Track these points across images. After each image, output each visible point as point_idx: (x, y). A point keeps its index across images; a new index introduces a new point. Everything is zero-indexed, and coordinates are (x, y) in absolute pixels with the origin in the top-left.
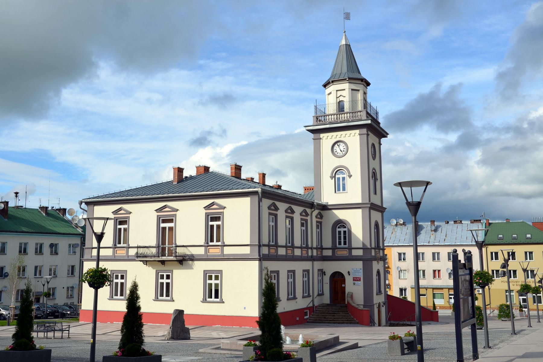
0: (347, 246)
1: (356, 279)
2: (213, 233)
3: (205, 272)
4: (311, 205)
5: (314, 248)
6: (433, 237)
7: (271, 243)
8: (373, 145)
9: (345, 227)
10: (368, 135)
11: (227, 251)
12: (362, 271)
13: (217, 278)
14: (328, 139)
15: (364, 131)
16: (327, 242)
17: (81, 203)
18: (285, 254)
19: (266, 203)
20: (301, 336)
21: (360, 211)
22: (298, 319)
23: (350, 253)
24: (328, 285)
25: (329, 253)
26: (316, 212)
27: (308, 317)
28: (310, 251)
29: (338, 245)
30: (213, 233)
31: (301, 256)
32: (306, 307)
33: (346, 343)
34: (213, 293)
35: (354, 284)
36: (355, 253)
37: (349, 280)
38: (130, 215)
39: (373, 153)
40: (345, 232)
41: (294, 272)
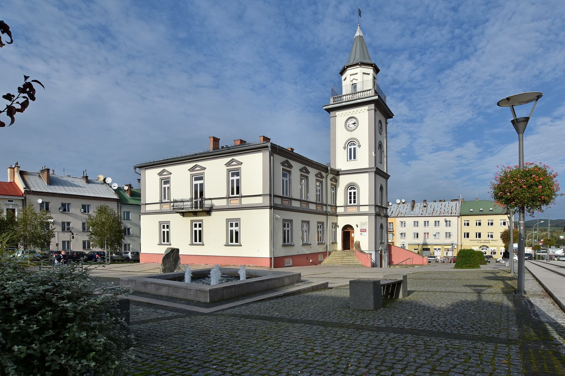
0: (356, 204)
1: (363, 231)
2: (235, 189)
3: (228, 220)
4: (325, 169)
5: (329, 205)
6: (425, 211)
8: (380, 122)
10: (375, 110)
11: (245, 201)
13: (237, 225)
14: (341, 116)
15: (372, 106)
16: (312, 198)
17: (135, 168)
18: (315, 209)
19: (279, 159)
21: (367, 174)
22: (311, 261)
23: (359, 209)
26: (330, 176)
28: (324, 207)
30: (235, 189)
34: (234, 238)
35: (361, 234)
39: (379, 128)
40: (355, 193)
41: (308, 222)
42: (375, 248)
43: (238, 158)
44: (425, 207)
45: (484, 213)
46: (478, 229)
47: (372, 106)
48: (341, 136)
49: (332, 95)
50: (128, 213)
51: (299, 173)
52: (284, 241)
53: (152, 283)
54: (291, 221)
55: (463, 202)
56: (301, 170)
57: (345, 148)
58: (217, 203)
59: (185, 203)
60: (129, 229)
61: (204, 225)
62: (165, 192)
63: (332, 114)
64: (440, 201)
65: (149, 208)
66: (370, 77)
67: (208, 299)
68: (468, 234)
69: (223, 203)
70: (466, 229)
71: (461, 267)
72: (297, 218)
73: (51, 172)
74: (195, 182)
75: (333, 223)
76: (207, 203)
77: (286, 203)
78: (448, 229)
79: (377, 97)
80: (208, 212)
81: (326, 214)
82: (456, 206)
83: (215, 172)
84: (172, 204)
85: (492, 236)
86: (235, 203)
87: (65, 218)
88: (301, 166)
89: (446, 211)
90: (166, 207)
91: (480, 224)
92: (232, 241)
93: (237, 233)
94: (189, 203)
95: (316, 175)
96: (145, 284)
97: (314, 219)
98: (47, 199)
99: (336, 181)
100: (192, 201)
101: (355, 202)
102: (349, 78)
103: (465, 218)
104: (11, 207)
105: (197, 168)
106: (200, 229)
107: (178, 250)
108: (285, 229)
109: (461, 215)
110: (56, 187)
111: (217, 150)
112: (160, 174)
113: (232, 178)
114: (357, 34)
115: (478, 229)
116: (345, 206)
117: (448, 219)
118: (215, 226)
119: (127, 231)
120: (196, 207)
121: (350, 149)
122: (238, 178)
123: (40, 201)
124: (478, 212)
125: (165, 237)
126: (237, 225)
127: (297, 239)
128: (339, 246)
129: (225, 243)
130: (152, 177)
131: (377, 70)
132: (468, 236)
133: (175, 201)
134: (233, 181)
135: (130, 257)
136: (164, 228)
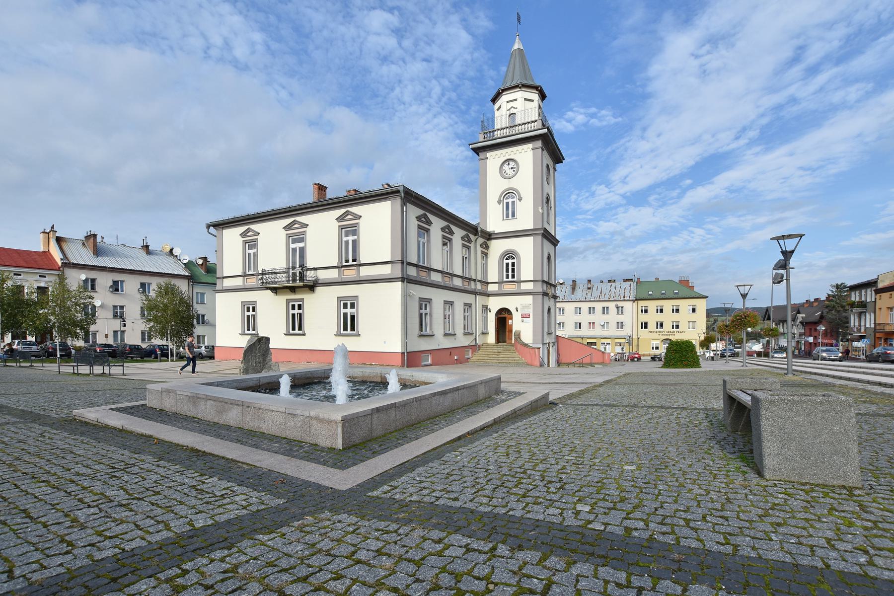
1: (525, 316)
5: (479, 281)
6: (589, 294)
11: (365, 272)
13: (353, 306)
14: (495, 158)
15: (539, 144)
17: (208, 226)
19: (414, 212)
20: (341, 399)
33: (519, 394)
34: (349, 324)
36: (525, 287)
37: (516, 317)
38: (259, 237)
39: (546, 175)
40: (513, 264)
41: (451, 303)
42: (543, 340)
44: (589, 288)
45: (667, 296)
46: (660, 318)
47: (539, 144)
48: (495, 185)
49: (482, 130)
50: (203, 294)
51: (441, 233)
53: (207, 398)
54: (429, 301)
55: (638, 282)
56: (443, 229)
57: (499, 202)
58: (323, 275)
59: (278, 275)
60: (203, 316)
61: (306, 306)
62: (249, 260)
63: (482, 155)
64: (609, 281)
65: (227, 283)
66: (535, 104)
67: (340, 441)
68: (646, 324)
69: (333, 274)
70: (643, 318)
71: (675, 366)
72: (438, 297)
73: (99, 239)
74: (292, 246)
75: (483, 306)
76: (310, 275)
77: (423, 275)
78: (620, 318)
79: (546, 130)
80: (311, 287)
81: (475, 293)
82: (630, 289)
83: (322, 233)
84: (260, 277)
85: (677, 327)
86: (350, 274)
87: (117, 300)
88: (444, 223)
89: (617, 294)
90: (252, 282)
91: (661, 311)
92: (345, 329)
93: (353, 317)
94: (284, 275)
95: (462, 238)
96: (195, 399)
97: (459, 299)
98: (92, 275)
99: (487, 247)
100: (288, 272)
101: (513, 276)
102: (504, 112)
103: (641, 303)
104: (43, 285)
105: (296, 226)
106: (300, 311)
107: (268, 339)
109: (637, 300)
110: (106, 259)
111: (322, 202)
112: (243, 235)
113: (346, 239)
114: (516, 47)
115: (660, 318)
116: (500, 283)
117: (620, 304)
118: (321, 308)
119: (201, 319)
120: (294, 280)
121: (507, 204)
122: (355, 238)
123: (83, 277)
124: (672, 296)
125: (250, 322)
126: (353, 306)
127: (437, 326)
128: (491, 338)
129: (335, 331)
130: (232, 237)
131: (543, 96)
132: (646, 327)
133: (265, 273)
134: (347, 243)
135: (205, 353)
136: (248, 311)
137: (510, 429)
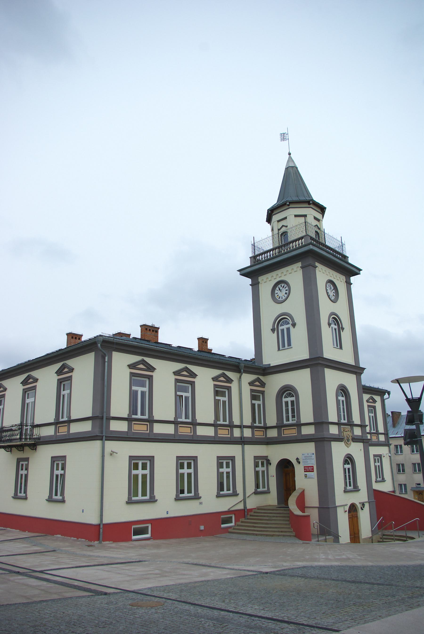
7: (372, 431)
9: (348, 464)
12: (314, 457)
14: (267, 282)
16: (272, 419)
18: (173, 432)
22: (202, 528)
23: (299, 431)
24: (275, 477)
25: (273, 433)
27: (233, 524)
29: (285, 422)
31: (174, 435)
32: (226, 509)
35: (306, 476)
37: (299, 470)
43: (194, 368)
52: (257, 486)
57: (273, 330)
80: (34, 446)
108: (257, 469)
137: (152, 597)
